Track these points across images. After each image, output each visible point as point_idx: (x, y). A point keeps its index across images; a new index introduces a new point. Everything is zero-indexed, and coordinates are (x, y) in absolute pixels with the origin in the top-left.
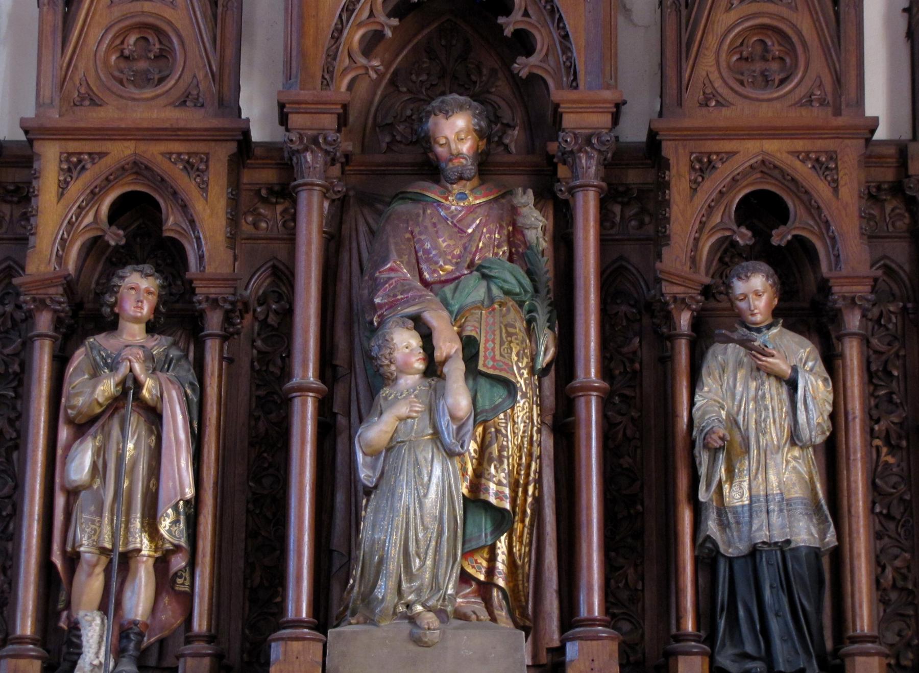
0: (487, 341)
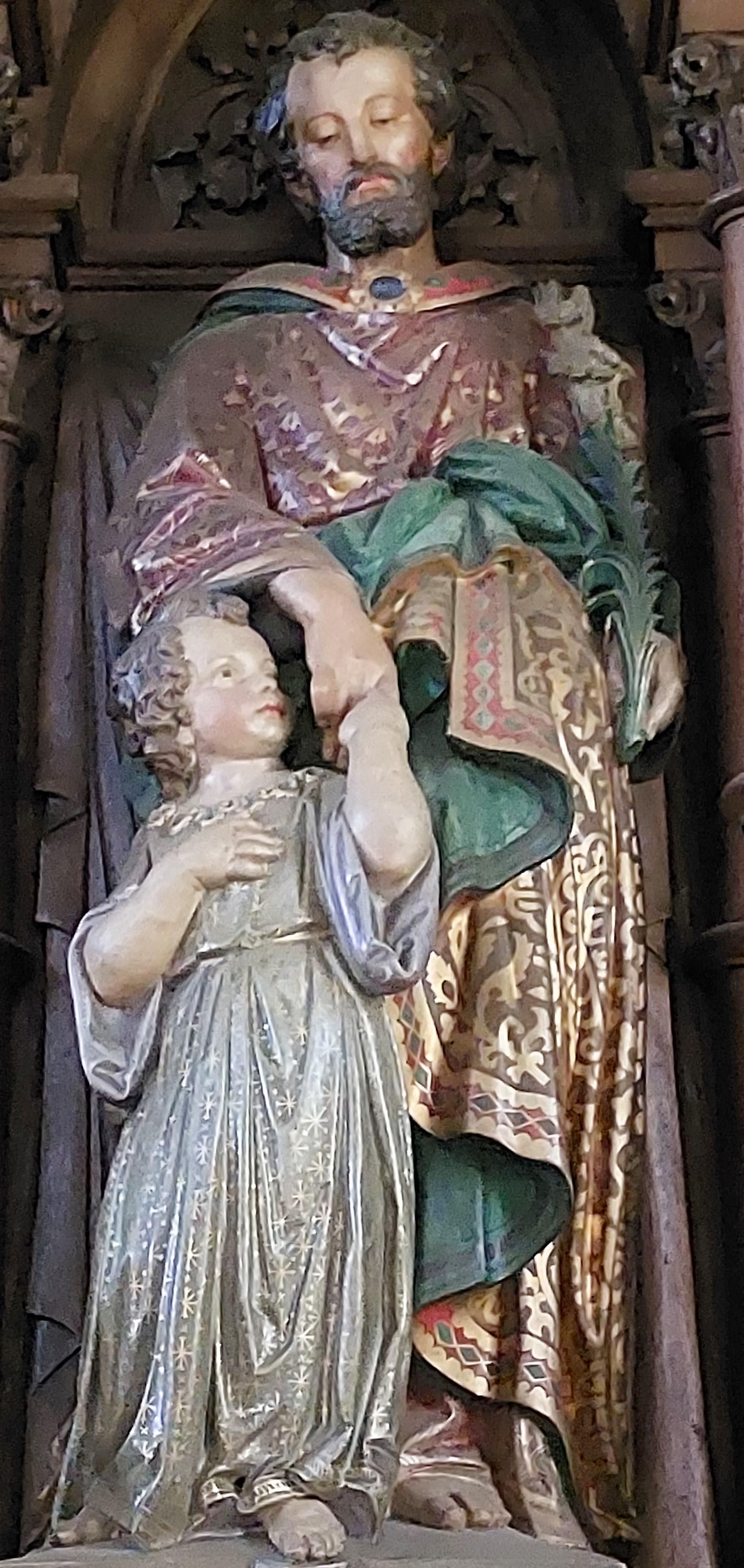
0: (471, 661)
